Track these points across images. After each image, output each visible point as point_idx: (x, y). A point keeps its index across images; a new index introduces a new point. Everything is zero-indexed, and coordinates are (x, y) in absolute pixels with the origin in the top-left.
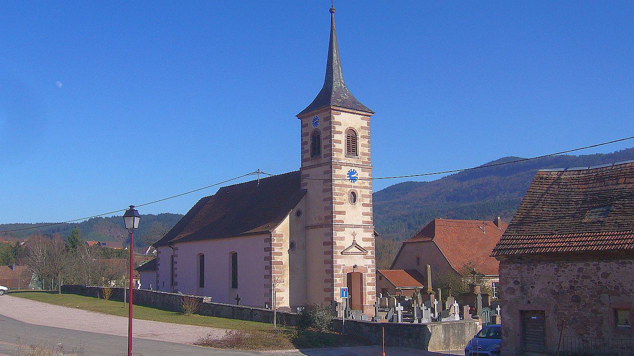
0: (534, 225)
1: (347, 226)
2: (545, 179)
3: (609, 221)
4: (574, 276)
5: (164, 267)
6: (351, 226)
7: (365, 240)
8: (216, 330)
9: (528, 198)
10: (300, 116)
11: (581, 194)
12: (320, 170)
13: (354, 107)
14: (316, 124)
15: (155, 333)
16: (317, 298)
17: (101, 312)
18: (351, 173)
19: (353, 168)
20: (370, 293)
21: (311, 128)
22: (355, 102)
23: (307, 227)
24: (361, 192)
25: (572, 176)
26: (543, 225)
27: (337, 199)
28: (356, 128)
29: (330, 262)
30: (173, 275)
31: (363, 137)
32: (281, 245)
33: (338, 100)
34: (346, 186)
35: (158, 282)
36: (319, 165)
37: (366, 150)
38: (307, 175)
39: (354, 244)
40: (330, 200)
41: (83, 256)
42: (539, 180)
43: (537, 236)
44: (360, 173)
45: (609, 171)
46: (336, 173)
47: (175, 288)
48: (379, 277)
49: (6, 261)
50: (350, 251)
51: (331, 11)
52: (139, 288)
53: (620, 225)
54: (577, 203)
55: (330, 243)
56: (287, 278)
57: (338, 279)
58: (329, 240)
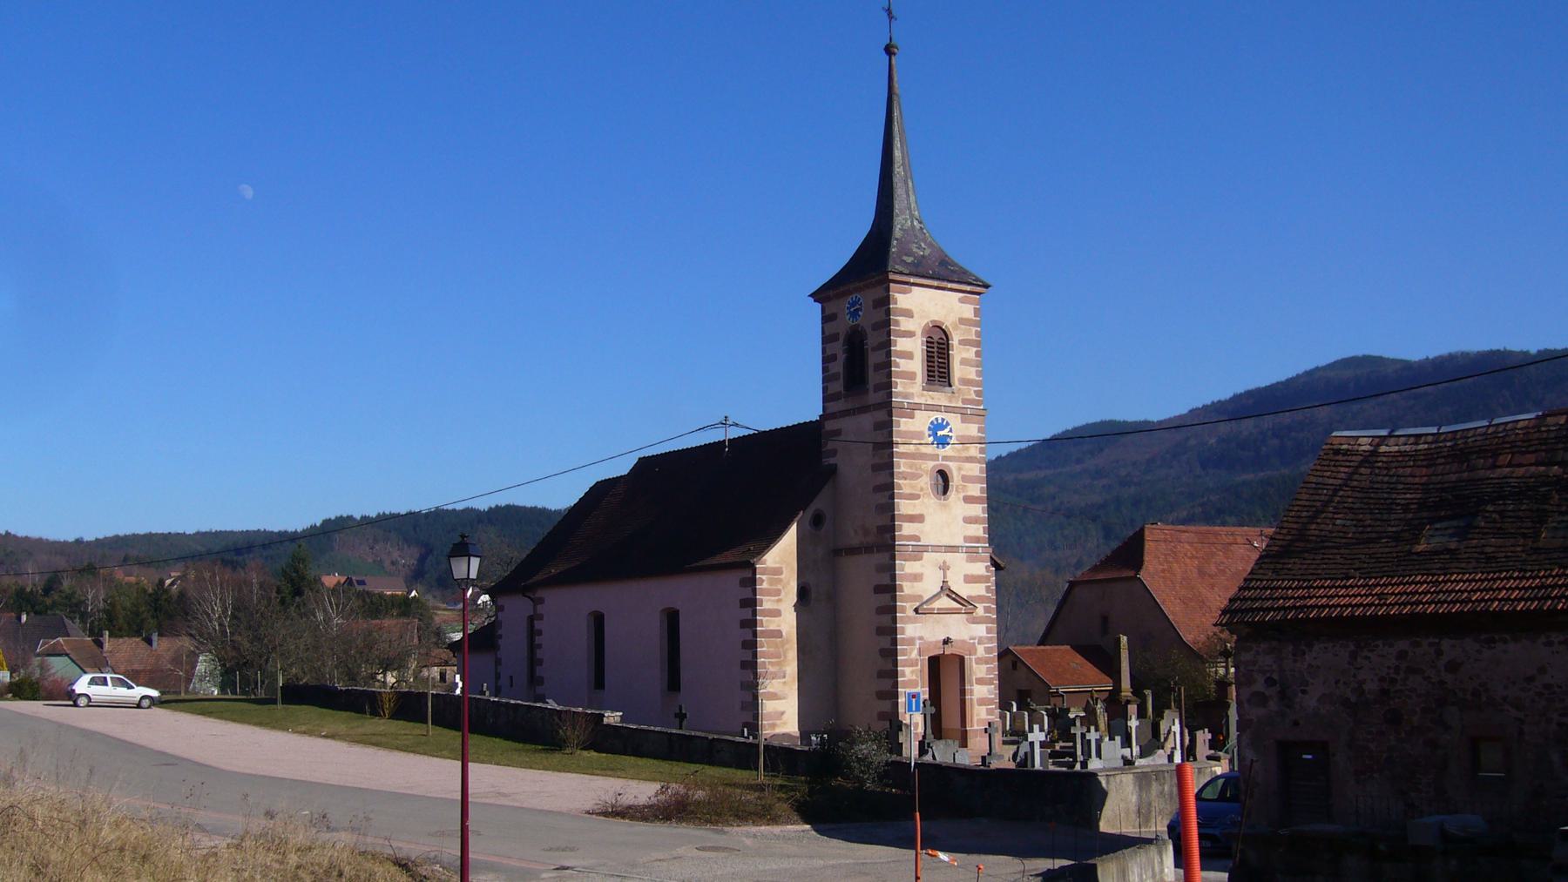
0: (1312, 556)
1: (925, 548)
2: (1344, 455)
3: (1469, 550)
4: (1389, 668)
5: (512, 643)
6: (937, 548)
7: (970, 579)
8: (633, 783)
9: (1306, 497)
10: (818, 296)
11: (1418, 489)
12: (866, 420)
13: (944, 273)
14: (855, 314)
15: (503, 790)
16: (862, 716)
17: (377, 744)
18: (936, 427)
19: (940, 416)
20: (982, 702)
21: (845, 322)
22: (945, 262)
23: (837, 552)
24: (960, 469)
25: (1403, 448)
26: (1331, 556)
27: (903, 485)
28: (948, 324)
29: (889, 631)
30: (533, 662)
31: (963, 342)
32: (778, 592)
33: (905, 258)
34: (924, 457)
35: (498, 676)
36: (864, 409)
37: (972, 373)
38: (838, 433)
39: (946, 590)
40: (888, 488)
41: (320, 617)
42: (1331, 456)
43: (1315, 581)
44: (957, 427)
45: (1479, 438)
46: (902, 428)
47: (539, 690)
48: (1008, 661)
49: (135, 627)
50: (937, 605)
51: (889, 50)
52: (458, 692)
53: (1490, 559)
54: (1406, 508)
55: (889, 589)
56: (792, 668)
57: (908, 670)
58: (886, 581)
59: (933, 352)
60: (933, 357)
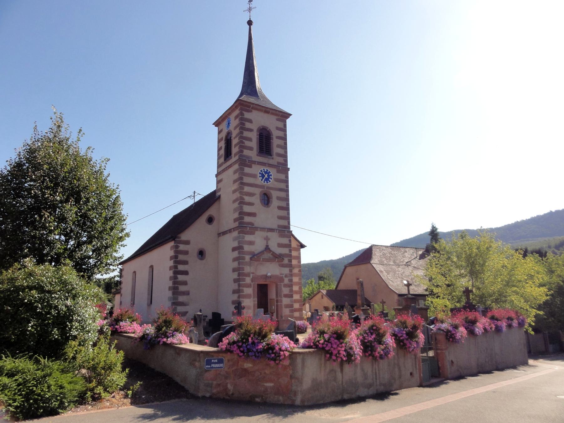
1: (256, 229)
6: (263, 229)
23: (219, 235)
39: (267, 249)
51: (250, 23)
59: (263, 142)
60: (263, 142)
